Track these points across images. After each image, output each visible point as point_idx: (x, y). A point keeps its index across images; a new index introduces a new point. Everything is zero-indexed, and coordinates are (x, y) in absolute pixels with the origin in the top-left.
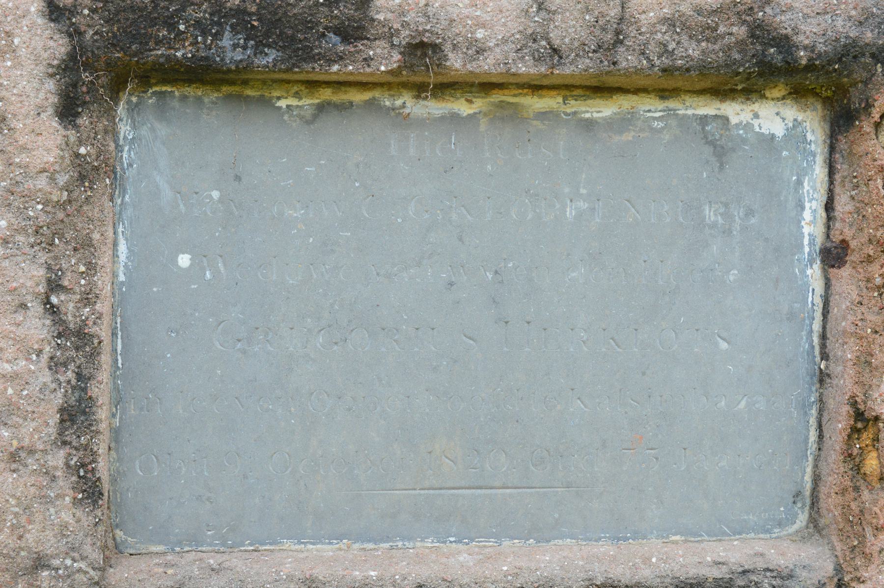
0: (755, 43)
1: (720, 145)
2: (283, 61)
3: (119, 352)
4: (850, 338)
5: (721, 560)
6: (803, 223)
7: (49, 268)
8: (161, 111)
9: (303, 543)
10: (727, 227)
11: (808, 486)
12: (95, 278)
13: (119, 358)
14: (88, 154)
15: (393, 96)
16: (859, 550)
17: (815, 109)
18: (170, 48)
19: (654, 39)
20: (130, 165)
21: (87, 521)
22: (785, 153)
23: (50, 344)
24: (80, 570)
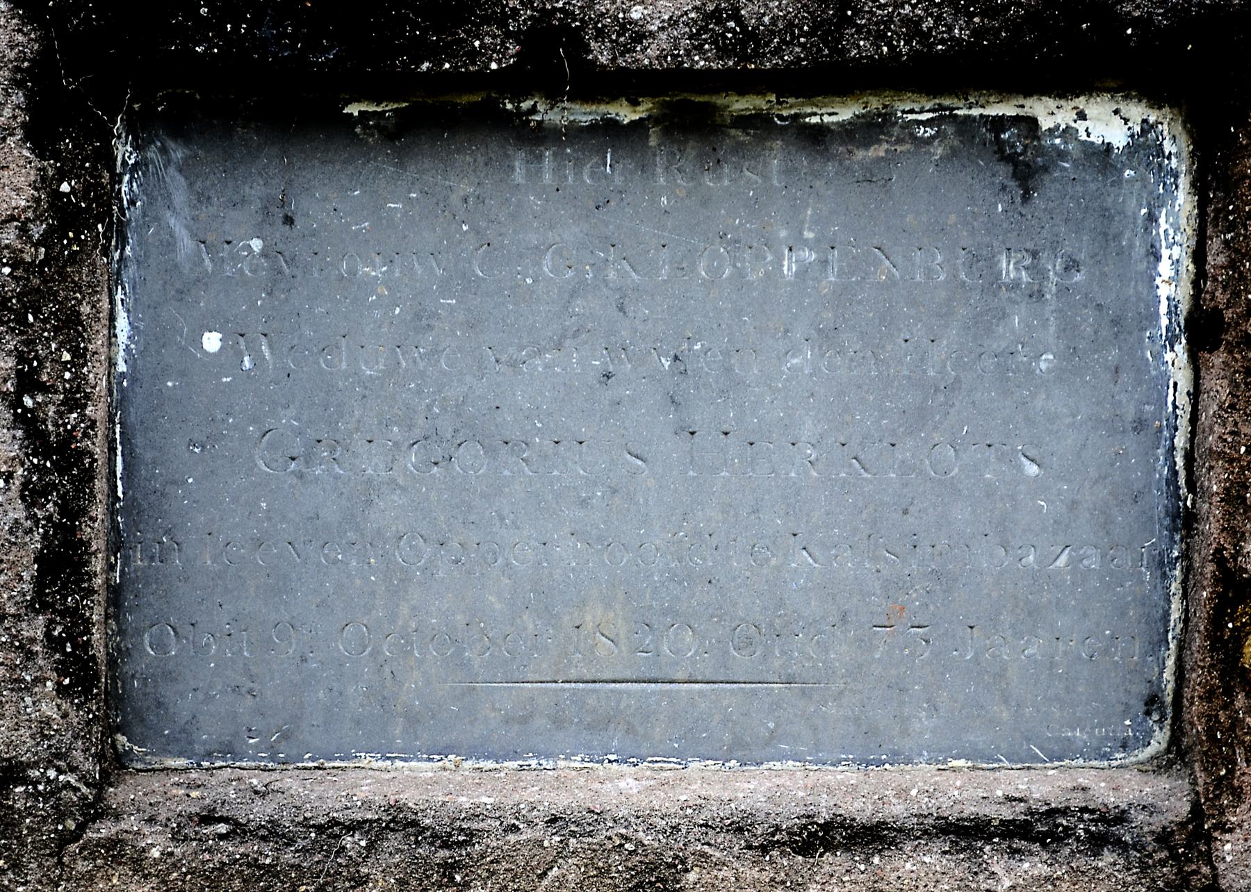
1: (1024, 162)
3: (119, 475)
4: (1217, 461)
5: (1017, 795)
6: (1158, 281)
7: (21, 358)
9: (388, 758)
10: (1036, 287)
13: (119, 483)
16: (1228, 787)
19: (899, 14)
20: (132, 202)
22: (1128, 173)
23: (22, 464)
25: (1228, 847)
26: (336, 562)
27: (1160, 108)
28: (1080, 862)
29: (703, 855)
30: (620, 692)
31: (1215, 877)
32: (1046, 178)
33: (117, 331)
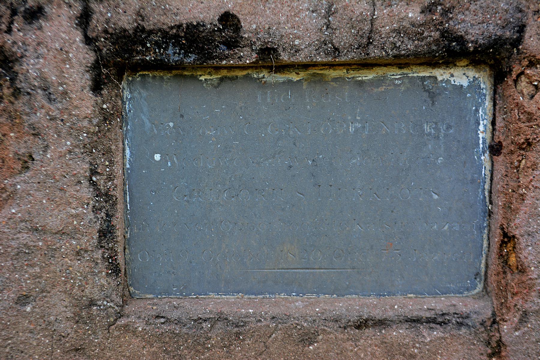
0: (444, 41)
1: (432, 92)
2: (198, 60)
5: (432, 308)
6: (479, 132)
7: (91, 164)
8: (143, 84)
10: (437, 135)
11: (483, 270)
12: (114, 168)
13: (128, 205)
14: (108, 108)
15: (258, 72)
17: (485, 71)
18: (143, 55)
20: (130, 111)
21: (113, 284)
24: (110, 307)
25: (505, 327)
26: (200, 230)
27: (479, 72)
28: (454, 332)
29: (324, 330)
30: (297, 273)
31: (500, 337)
32: (440, 97)
33: (126, 154)
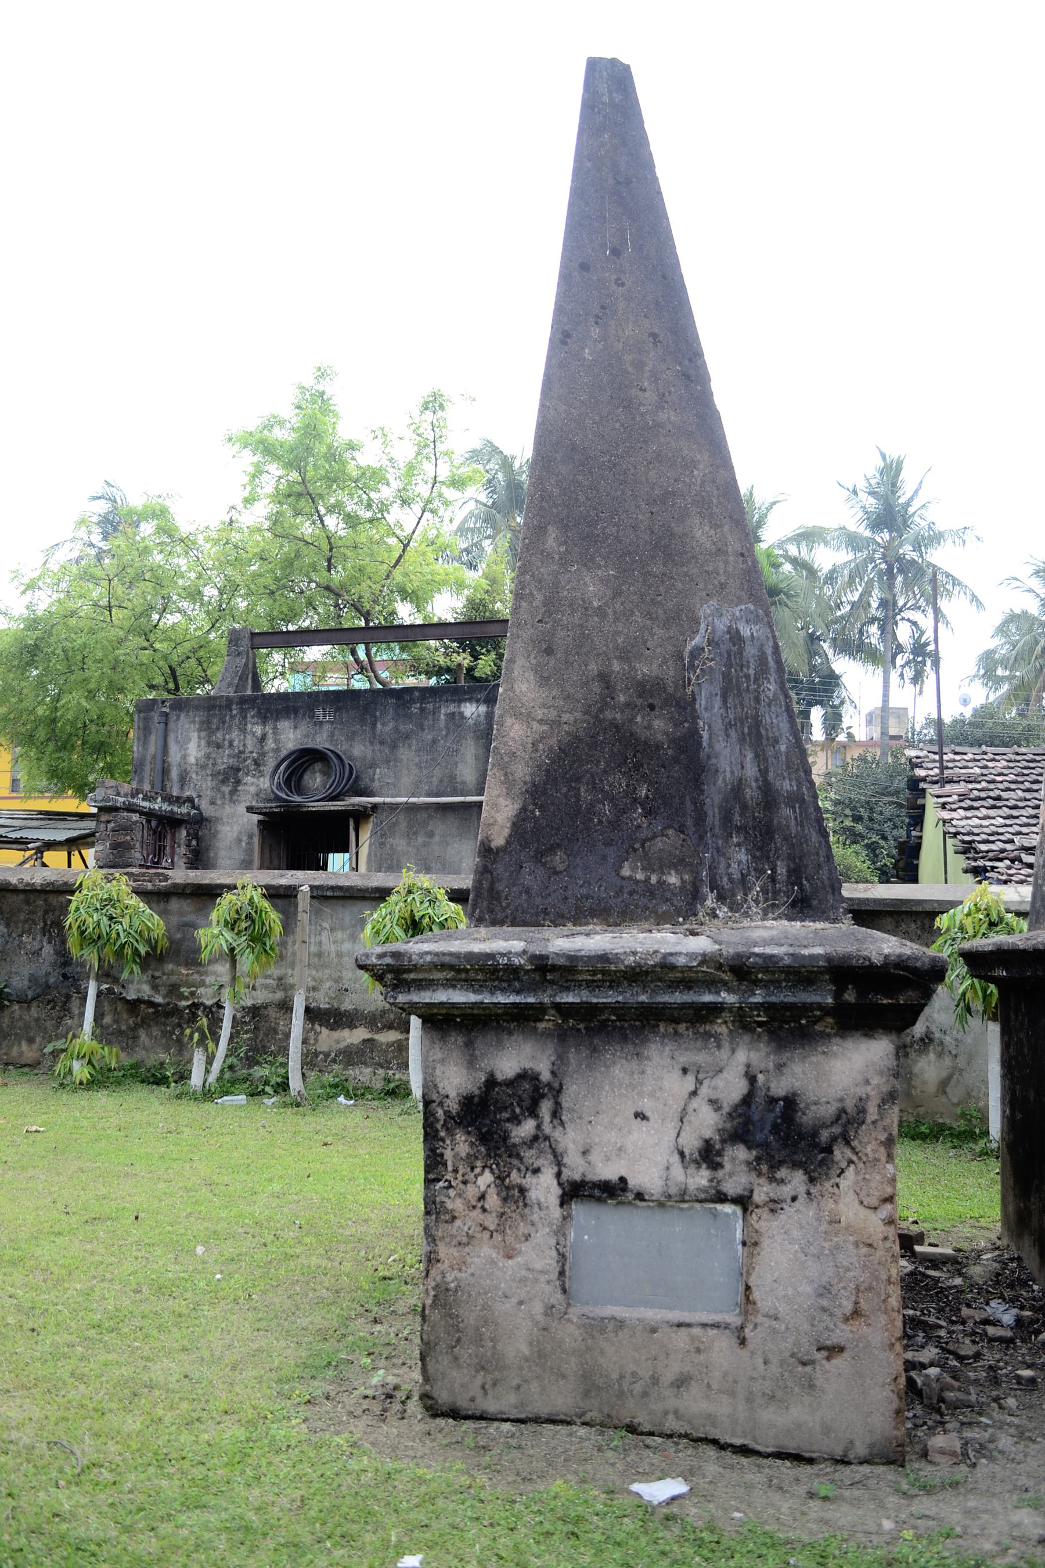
1: (715, 1215)
